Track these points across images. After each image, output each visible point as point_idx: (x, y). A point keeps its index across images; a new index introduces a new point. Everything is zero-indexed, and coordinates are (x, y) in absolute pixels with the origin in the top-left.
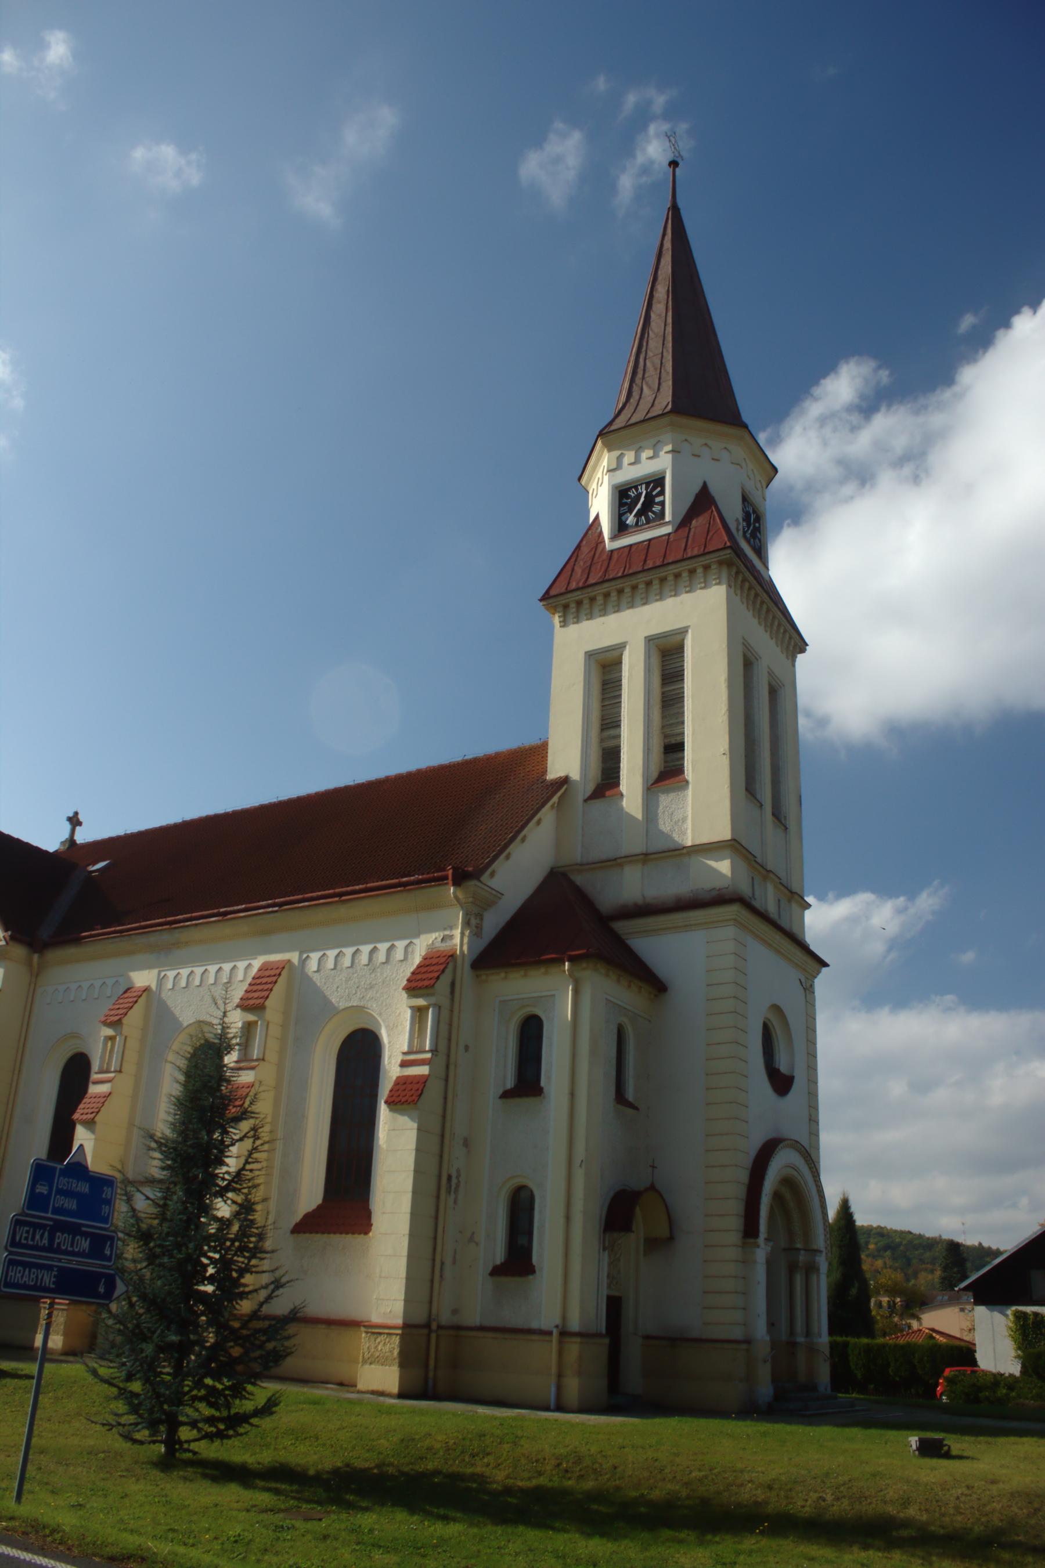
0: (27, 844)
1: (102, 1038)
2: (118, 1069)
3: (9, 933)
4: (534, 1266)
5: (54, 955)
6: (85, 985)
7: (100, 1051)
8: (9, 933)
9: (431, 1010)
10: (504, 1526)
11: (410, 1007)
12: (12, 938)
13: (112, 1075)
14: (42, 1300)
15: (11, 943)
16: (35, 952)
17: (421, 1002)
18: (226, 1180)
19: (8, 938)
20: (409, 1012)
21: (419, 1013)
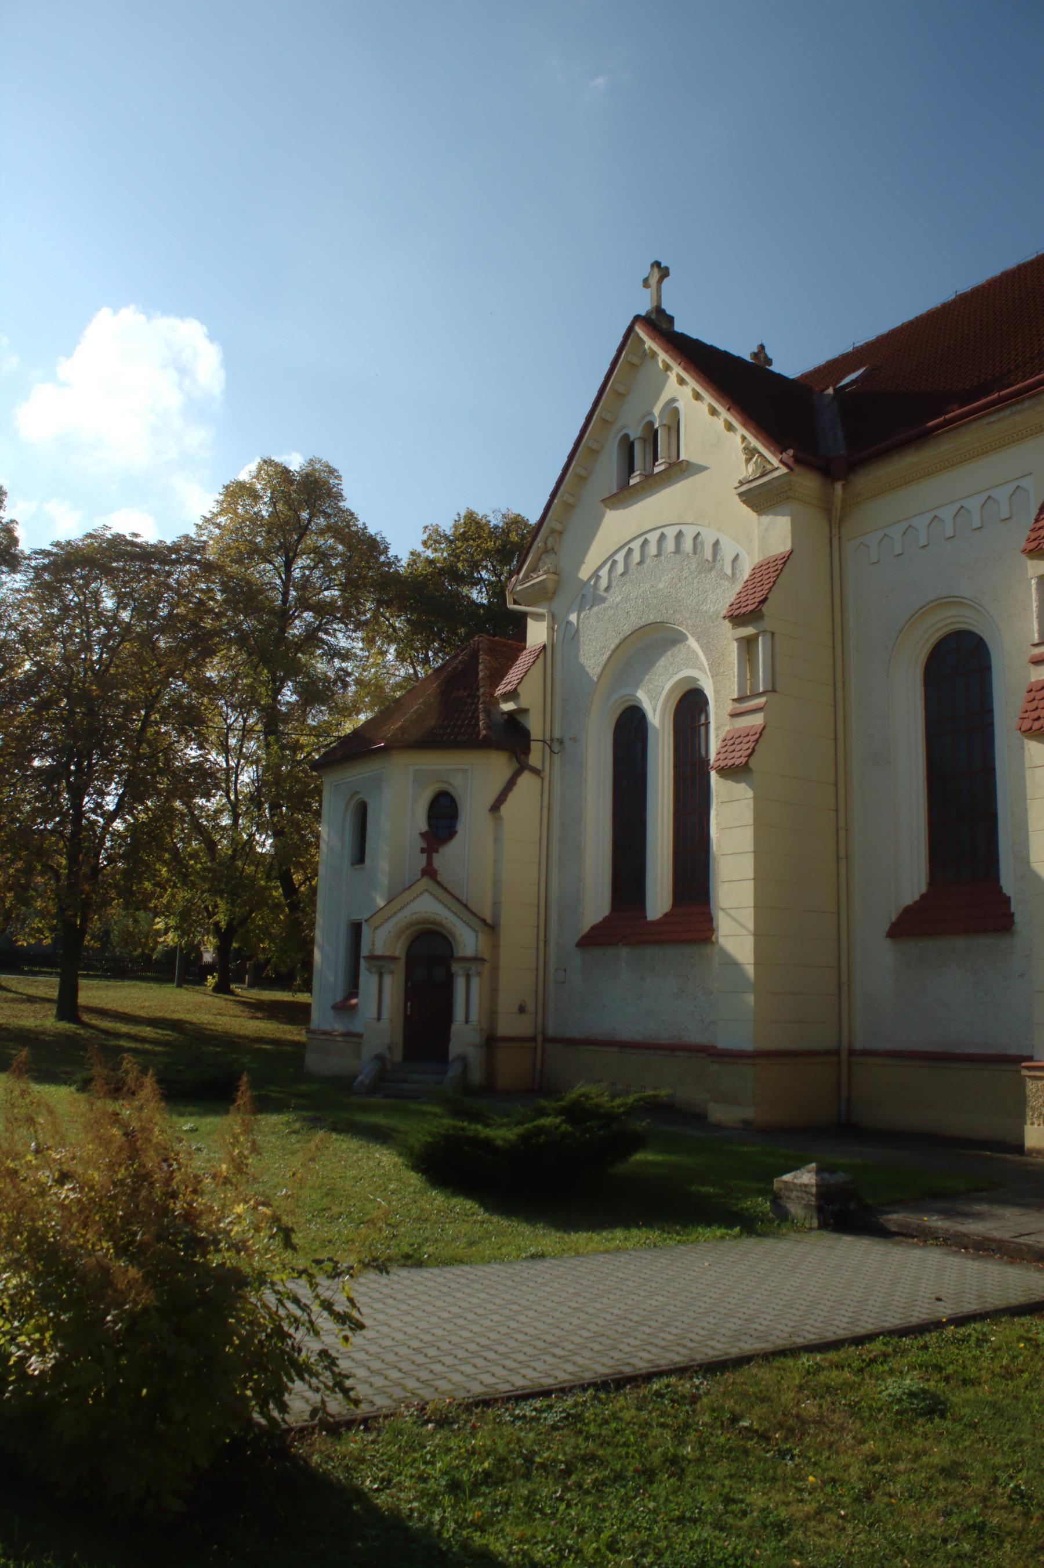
0: (711, 347)
1: (1033, 582)
2: (770, 688)
3: (791, 452)
4: (1007, 900)
5: (864, 480)
6: (947, 514)
7: (1035, 604)
8: (791, 452)
9: (760, 638)
10: (163, 1104)
11: (737, 640)
12: (797, 460)
13: (762, 700)
14: (1024, 1064)
15: (797, 469)
16: (835, 479)
17: (749, 631)
18: (300, 886)
19: (790, 462)
20: (735, 644)
21: (748, 645)
